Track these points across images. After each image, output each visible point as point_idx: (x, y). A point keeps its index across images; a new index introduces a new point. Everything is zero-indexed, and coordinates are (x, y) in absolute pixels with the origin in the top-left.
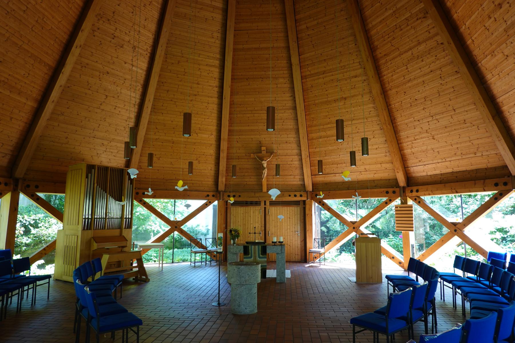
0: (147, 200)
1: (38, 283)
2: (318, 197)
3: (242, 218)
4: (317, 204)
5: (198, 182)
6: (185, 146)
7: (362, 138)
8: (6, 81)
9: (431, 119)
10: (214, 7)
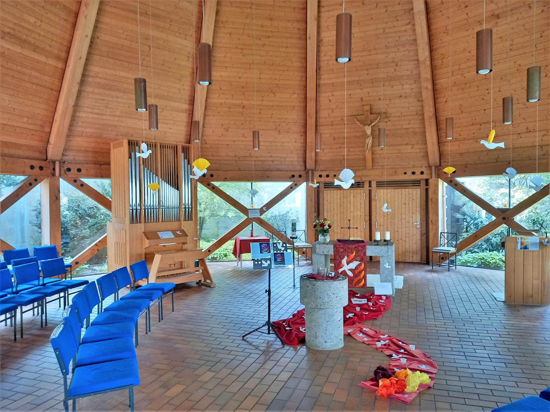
0: (216, 184)
1: (48, 299)
2: (482, 142)
3: (339, 205)
4: (446, 184)
5: (279, 159)
6: (259, 111)
8: (12, 32)
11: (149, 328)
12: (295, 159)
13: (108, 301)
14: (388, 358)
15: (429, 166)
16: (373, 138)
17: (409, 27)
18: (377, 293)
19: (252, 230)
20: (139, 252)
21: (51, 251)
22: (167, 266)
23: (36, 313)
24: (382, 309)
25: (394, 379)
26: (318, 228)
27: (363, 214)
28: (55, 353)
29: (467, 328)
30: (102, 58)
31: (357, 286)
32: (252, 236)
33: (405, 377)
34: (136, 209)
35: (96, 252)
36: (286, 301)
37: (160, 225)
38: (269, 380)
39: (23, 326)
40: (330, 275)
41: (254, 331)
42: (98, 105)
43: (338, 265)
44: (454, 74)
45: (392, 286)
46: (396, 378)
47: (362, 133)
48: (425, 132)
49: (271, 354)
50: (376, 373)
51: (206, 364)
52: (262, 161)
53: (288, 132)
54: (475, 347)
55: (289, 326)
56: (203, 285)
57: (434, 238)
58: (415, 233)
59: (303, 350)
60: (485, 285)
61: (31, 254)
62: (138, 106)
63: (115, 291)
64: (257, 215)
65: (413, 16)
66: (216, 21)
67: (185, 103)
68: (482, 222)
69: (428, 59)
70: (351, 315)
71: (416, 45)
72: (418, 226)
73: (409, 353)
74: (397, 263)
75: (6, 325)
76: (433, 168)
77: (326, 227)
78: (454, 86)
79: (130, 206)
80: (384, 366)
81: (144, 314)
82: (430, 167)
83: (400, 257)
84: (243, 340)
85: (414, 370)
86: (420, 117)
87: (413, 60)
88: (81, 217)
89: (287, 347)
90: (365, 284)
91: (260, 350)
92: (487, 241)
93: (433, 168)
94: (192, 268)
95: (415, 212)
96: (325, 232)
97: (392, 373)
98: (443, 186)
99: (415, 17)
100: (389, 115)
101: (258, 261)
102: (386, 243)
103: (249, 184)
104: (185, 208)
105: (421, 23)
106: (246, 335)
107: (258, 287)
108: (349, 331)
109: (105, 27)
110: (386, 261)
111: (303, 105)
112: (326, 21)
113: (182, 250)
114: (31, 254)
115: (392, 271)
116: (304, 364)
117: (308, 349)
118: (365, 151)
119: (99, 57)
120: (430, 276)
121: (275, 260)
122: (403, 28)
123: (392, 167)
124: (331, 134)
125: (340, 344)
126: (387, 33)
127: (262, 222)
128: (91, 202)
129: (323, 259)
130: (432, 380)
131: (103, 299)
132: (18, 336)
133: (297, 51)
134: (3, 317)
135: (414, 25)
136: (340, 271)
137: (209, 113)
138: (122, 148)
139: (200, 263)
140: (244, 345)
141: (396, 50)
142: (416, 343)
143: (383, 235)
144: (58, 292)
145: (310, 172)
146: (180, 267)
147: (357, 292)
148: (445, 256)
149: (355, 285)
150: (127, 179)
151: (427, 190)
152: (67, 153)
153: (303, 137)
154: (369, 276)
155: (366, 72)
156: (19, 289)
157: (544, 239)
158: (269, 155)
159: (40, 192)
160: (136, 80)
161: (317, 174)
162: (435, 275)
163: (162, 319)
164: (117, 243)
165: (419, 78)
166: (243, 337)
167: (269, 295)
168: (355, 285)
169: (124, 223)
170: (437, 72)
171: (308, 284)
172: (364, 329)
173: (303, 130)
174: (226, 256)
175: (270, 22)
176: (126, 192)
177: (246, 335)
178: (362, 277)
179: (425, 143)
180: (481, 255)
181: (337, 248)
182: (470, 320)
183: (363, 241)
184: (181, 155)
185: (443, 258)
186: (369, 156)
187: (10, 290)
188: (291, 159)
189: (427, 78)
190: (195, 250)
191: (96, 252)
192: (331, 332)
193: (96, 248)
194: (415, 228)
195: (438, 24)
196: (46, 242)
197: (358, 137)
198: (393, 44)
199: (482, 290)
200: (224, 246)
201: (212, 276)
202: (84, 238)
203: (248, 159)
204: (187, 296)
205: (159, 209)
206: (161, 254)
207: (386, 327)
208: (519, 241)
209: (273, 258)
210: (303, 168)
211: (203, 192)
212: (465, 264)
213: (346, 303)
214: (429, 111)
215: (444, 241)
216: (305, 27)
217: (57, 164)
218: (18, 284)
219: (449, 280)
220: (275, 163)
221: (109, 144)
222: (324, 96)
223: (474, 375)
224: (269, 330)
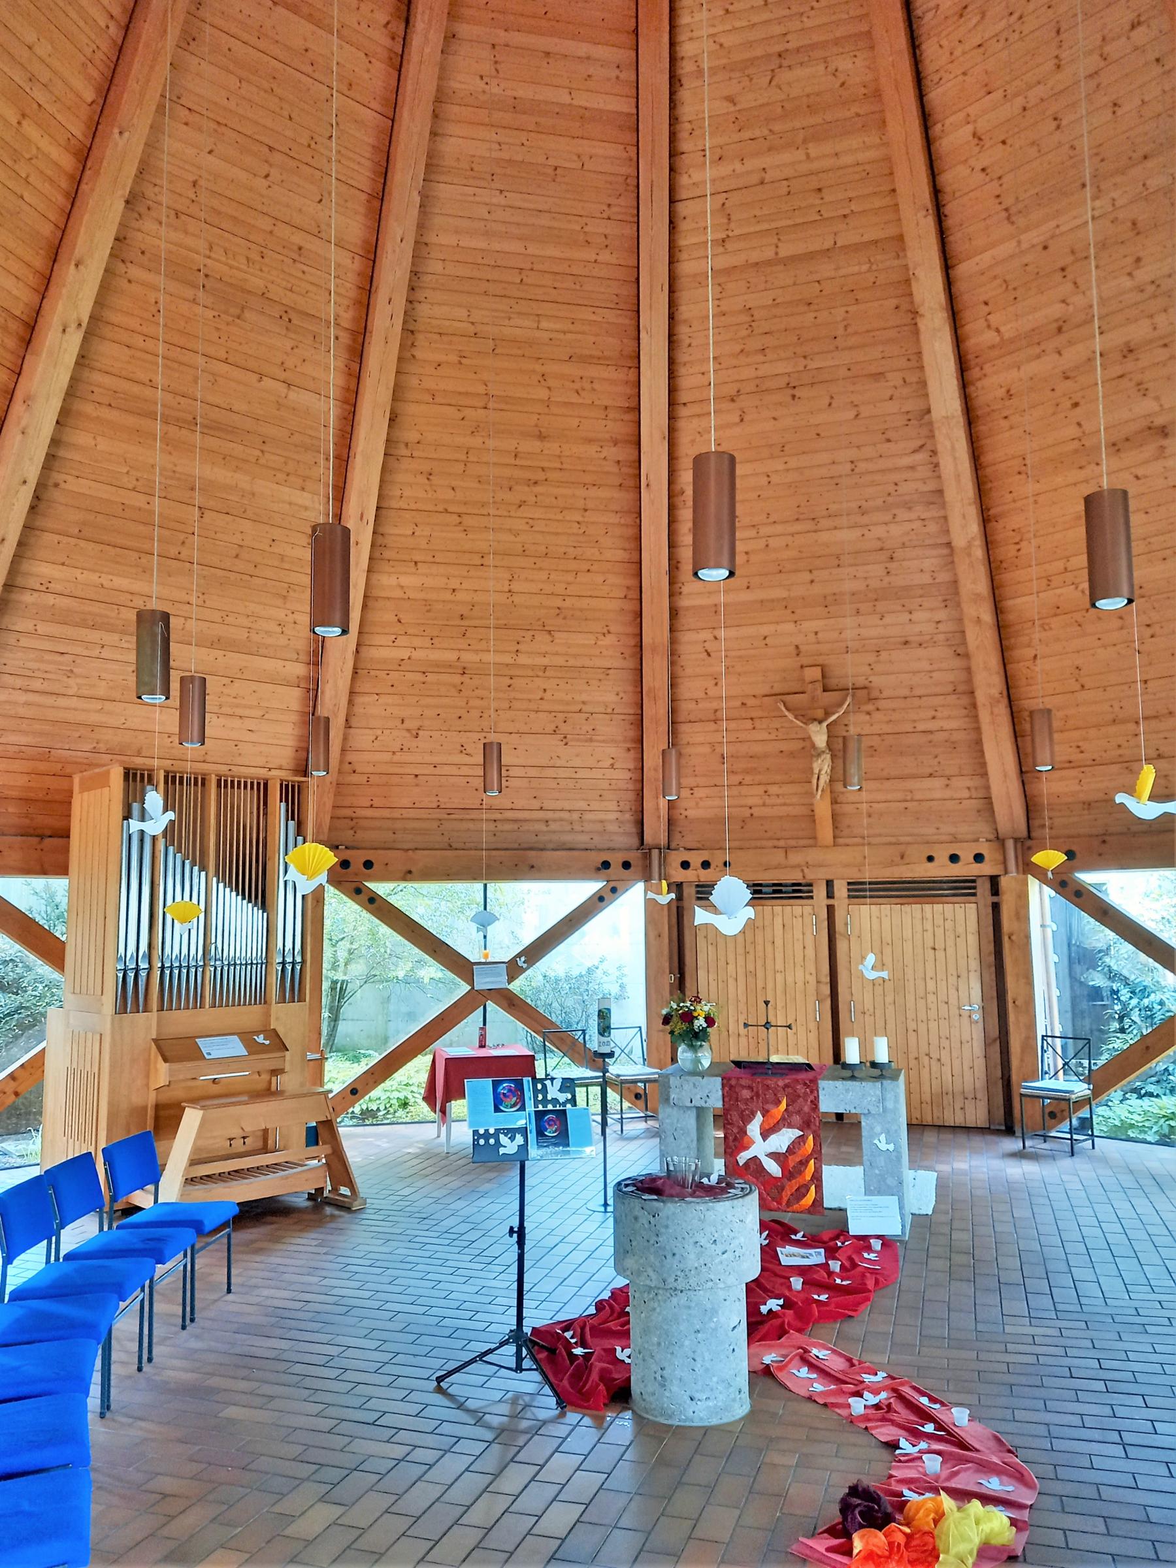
0: (381, 888)
3: (740, 950)
4: (1048, 892)
5: (566, 815)
10: (585, 116)
11: (150, 1352)
12: (612, 816)
14: (884, 1454)
15: (998, 838)
16: (833, 757)
17: (921, 457)
18: (856, 1228)
19: (483, 1029)
20: (137, 1100)
25: (899, 1531)
26: (680, 1025)
27: (812, 980)
29: (1127, 1346)
30: (65, 540)
31: (796, 1207)
33: (936, 1522)
34: (137, 970)
36: (578, 1257)
37: (207, 1017)
40: (705, 1181)
41: (473, 1361)
42: (43, 666)
43: (735, 1142)
44: (1053, 585)
45: (901, 1208)
46: (908, 1525)
47: (801, 744)
48: (979, 742)
51: (317, 1477)
52: (515, 821)
53: (591, 740)
55: (583, 1344)
56: (329, 1202)
57: (1023, 1052)
58: (966, 1036)
59: (622, 1426)
63: (48, 1231)
64: (499, 981)
65: (931, 431)
67: (297, 661)
68: (1161, 1003)
69: (978, 543)
70: (773, 1304)
71: (943, 505)
72: (976, 1017)
73: (948, 1435)
74: (915, 1127)
76: (1010, 844)
77: (700, 1023)
78: (1056, 615)
79: (118, 959)
80: (870, 1482)
81: (136, 1305)
83: (927, 1109)
84: (439, 1390)
85: (962, 1496)
86: (965, 700)
87: (935, 546)
89: (572, 1417)
90: (818, 1201)
91: (489, 1427)
93: (1010, 844)
94: (297, 1147)
95: (964, 974)
96: (695, 1037)
97: (892, 1504)
98: (1041, 900)
99: (937, 433)
100: (875, 694)
101: (487, 1135)
102: (878, 1071)
103: (478, 886)
104: (283, 963)
105: (953, 448)
106: (450, 1373)
108: (767, 1360)
109: (77, 457)
110: (878, 1129)
111: (631, 663)
112: (693, 442)
113: (269, 1093)
116: (624, 1477)
117: (640, 1422)
118: (813, 796)
119: (56, 538)
120: (1017, 1170)
121: (540, 1133)
122: (907, 461)
123: (893, 840)
124: (712, 745)
125: (737, 1405)
126: (861, 475)
127: (512, 1003)
129: (691, 1120)
130: (1019, 1530)
133: (614, 519)
135: (934, 452)
136: (743, 1157)
137: (364, 686)
138: (106, 790)
139: (321, 1134)
140: (440, 1407)
141: (889, 517)
142: (973, 1400)
145: (655, 853)
146: (260, 1144)
148: (1058, 1109)
149: (788, 1204)
150: (113, 878)
151: (996, 907)
153: (632, 754)
154: (828, 1171)
155: (807, 577)
158: (536, 804)
160: (140, 615)
161: (676, 858)
162: (1029, 1168)
163: (192, 1320)
164: (72, 1073)
165: (957, 593)
166: (440, 1379)
167: (521, 1243)
168: (788, 1204)
169: (99, 1012)
170: (1005, 577)
171: (637, 1212)
172: (815, 1351)
173: (632, 733)
174: (405, 1105)
175: (538, 443)
177: (450, 1373)
178: (808, 1178)
179: (984, 775)
181: (731, 1087)
182: (1138, 1320)
184: (279, 809)
185: (1052, 1115)
186: (823, 808)
188: (602, 816)
189: (978, 595)
192: (708, 1365)
194: (965, 1021)
195: (1004, 447)
197: (792, 755)
198: (879, 502)
200: (400, 1075)
203: (474, 815)
204: (277, 1240)
205: (204, 966)
206: (203, 1108)
207: (879, 1344)
209: (532, 1127)
210: (635, 841)
211: (341, 910)
212: (1120, 1133)
213: (752, 1268)
214: (988, 683)
215: (1051, 1060)
216: (635, 457)
219: (1074, 1185)
220: (553, 826)
222: (692, 641)
223: (1155, 1515)
224: (519, 1358)
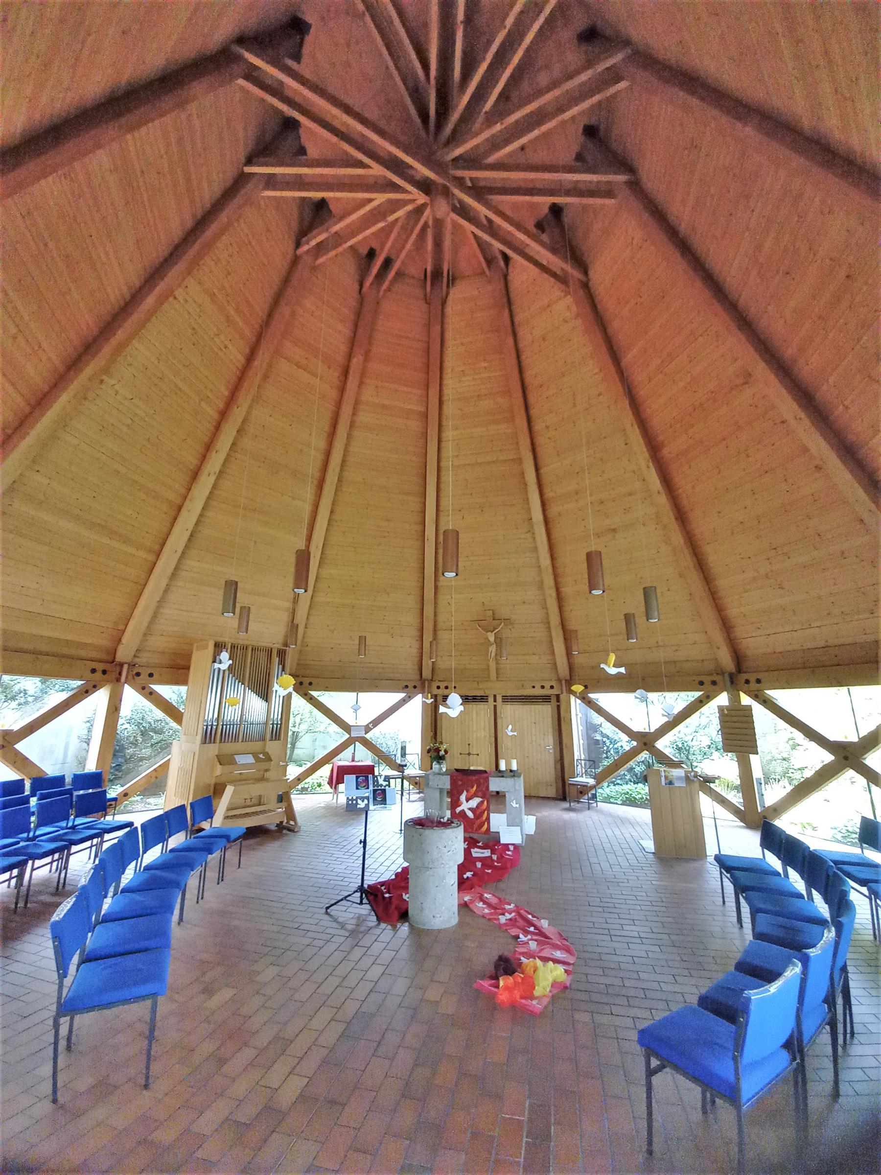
0: (315, 694)
1: (74, 849)
4: (579, 701)
7: (644, 589)
9: (773, 552)
13: (153, 855)
14: (510, 941)
18: (503, 841)
19: (354, 753)
21: (95, 780)
22: (241, 802)
23: (54, 867)
24: (509, 865)
25: (519, 976)
26: (434, 753)
28: (54, 943)
32: (353, 761)
34: (212, 725)
35: (153, 780)
37: (239, 746)
38: (352, 981)
39: (32, 888)
41: (342, 900)
43: (455, 803)
49: (361, 936)
50: (497, 967)
54: (623, 922)
56: (285, 828)
59: (404, 929)
60: (632, 830)
61: (68, 780)
62: (225, 610)
63: (163, 839)
64: (362, 734)
66: (330, 520)
70: (469, 874)
73: (540, 933)
75: (9, 887)
76: (564, 682)
77: (442, 753)
80: (507, 954)
82: (559, 680)
84: (327, 913)
85: (545, 960)
88: (143, 734)
92: (631, 770)
94: (272, 803)
96: (440, 759)
98: (576, 706)
101: (352, 800)
102: (512, 774)
107: (356, 831)
113: (263, 779)
114: (68, 780)
115: (521, 811)
116: (404, 953)
117: (412, 927)
121: (375, 799)
122: (523, 536)
127: (367, 743)
128: (159, 714)
131: (144, 852)
132: (21, 904)
134: (6, 876)
135: (534, 533)
136: (458, 810)
139: (284, 798)
143: (508, 764)
144: (91, 838)
147: (479, 839)
148: (583, 790)
149: (476, 830)
151: (558, 707)
152: (141, 655)
154: (493, 816)
156: (38, 833)
157: (690, 772)
159: (100, 698)
162: (572, 815)
166: (327, 908)
167: (364, 847)
173: (418, 634)
176: (202, 704)
180: (626, 788)
183: (485, 772)
184: (276, 660)
185: (581, 793)
186: (493, 665)
187: (25, 835)
190: (279, 780)
191: (153, 780)
193: (155, 774)
195: (557, 534)
196: (91, 767)
199: (627, 836)
201: (297, 815)
202: (142, 759)
207: (514, 891)
208: (663, 774)
210: (418, 677)
211: (298, 703)
213: (460, 859)
214: (555, 620)
215: (579, 769)
217: (126, 667)
218: (38, 826)
219: (590, 822)
221: (192, 645)
222: (443, 598)
